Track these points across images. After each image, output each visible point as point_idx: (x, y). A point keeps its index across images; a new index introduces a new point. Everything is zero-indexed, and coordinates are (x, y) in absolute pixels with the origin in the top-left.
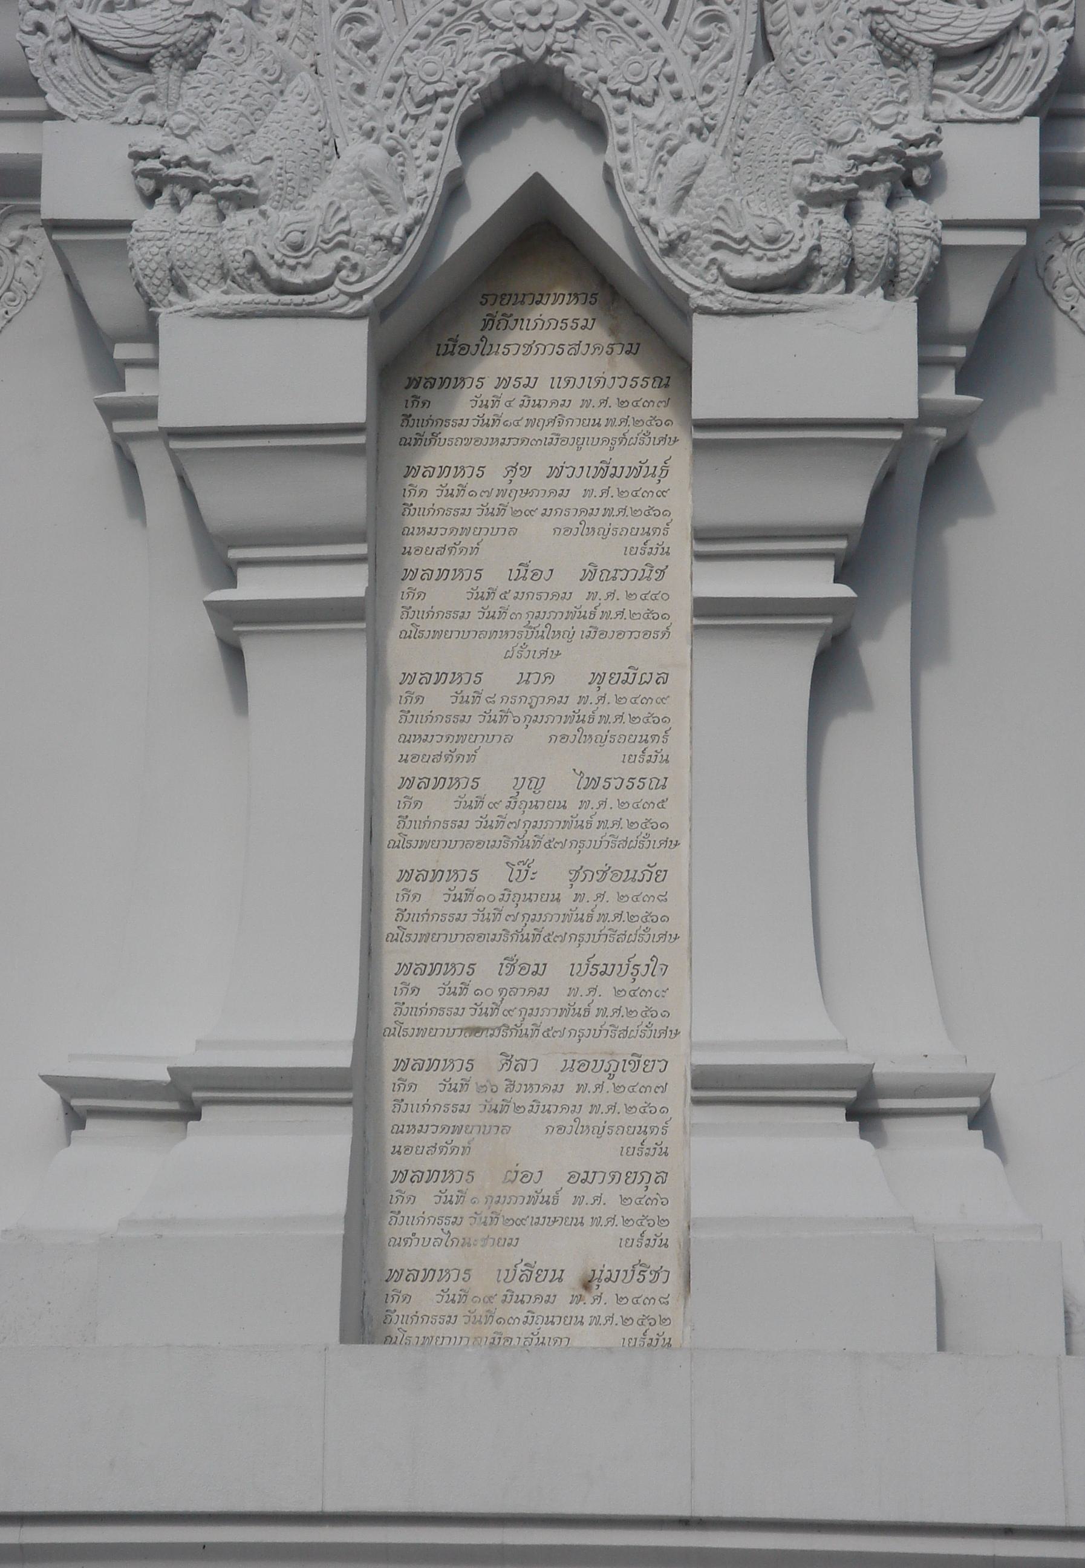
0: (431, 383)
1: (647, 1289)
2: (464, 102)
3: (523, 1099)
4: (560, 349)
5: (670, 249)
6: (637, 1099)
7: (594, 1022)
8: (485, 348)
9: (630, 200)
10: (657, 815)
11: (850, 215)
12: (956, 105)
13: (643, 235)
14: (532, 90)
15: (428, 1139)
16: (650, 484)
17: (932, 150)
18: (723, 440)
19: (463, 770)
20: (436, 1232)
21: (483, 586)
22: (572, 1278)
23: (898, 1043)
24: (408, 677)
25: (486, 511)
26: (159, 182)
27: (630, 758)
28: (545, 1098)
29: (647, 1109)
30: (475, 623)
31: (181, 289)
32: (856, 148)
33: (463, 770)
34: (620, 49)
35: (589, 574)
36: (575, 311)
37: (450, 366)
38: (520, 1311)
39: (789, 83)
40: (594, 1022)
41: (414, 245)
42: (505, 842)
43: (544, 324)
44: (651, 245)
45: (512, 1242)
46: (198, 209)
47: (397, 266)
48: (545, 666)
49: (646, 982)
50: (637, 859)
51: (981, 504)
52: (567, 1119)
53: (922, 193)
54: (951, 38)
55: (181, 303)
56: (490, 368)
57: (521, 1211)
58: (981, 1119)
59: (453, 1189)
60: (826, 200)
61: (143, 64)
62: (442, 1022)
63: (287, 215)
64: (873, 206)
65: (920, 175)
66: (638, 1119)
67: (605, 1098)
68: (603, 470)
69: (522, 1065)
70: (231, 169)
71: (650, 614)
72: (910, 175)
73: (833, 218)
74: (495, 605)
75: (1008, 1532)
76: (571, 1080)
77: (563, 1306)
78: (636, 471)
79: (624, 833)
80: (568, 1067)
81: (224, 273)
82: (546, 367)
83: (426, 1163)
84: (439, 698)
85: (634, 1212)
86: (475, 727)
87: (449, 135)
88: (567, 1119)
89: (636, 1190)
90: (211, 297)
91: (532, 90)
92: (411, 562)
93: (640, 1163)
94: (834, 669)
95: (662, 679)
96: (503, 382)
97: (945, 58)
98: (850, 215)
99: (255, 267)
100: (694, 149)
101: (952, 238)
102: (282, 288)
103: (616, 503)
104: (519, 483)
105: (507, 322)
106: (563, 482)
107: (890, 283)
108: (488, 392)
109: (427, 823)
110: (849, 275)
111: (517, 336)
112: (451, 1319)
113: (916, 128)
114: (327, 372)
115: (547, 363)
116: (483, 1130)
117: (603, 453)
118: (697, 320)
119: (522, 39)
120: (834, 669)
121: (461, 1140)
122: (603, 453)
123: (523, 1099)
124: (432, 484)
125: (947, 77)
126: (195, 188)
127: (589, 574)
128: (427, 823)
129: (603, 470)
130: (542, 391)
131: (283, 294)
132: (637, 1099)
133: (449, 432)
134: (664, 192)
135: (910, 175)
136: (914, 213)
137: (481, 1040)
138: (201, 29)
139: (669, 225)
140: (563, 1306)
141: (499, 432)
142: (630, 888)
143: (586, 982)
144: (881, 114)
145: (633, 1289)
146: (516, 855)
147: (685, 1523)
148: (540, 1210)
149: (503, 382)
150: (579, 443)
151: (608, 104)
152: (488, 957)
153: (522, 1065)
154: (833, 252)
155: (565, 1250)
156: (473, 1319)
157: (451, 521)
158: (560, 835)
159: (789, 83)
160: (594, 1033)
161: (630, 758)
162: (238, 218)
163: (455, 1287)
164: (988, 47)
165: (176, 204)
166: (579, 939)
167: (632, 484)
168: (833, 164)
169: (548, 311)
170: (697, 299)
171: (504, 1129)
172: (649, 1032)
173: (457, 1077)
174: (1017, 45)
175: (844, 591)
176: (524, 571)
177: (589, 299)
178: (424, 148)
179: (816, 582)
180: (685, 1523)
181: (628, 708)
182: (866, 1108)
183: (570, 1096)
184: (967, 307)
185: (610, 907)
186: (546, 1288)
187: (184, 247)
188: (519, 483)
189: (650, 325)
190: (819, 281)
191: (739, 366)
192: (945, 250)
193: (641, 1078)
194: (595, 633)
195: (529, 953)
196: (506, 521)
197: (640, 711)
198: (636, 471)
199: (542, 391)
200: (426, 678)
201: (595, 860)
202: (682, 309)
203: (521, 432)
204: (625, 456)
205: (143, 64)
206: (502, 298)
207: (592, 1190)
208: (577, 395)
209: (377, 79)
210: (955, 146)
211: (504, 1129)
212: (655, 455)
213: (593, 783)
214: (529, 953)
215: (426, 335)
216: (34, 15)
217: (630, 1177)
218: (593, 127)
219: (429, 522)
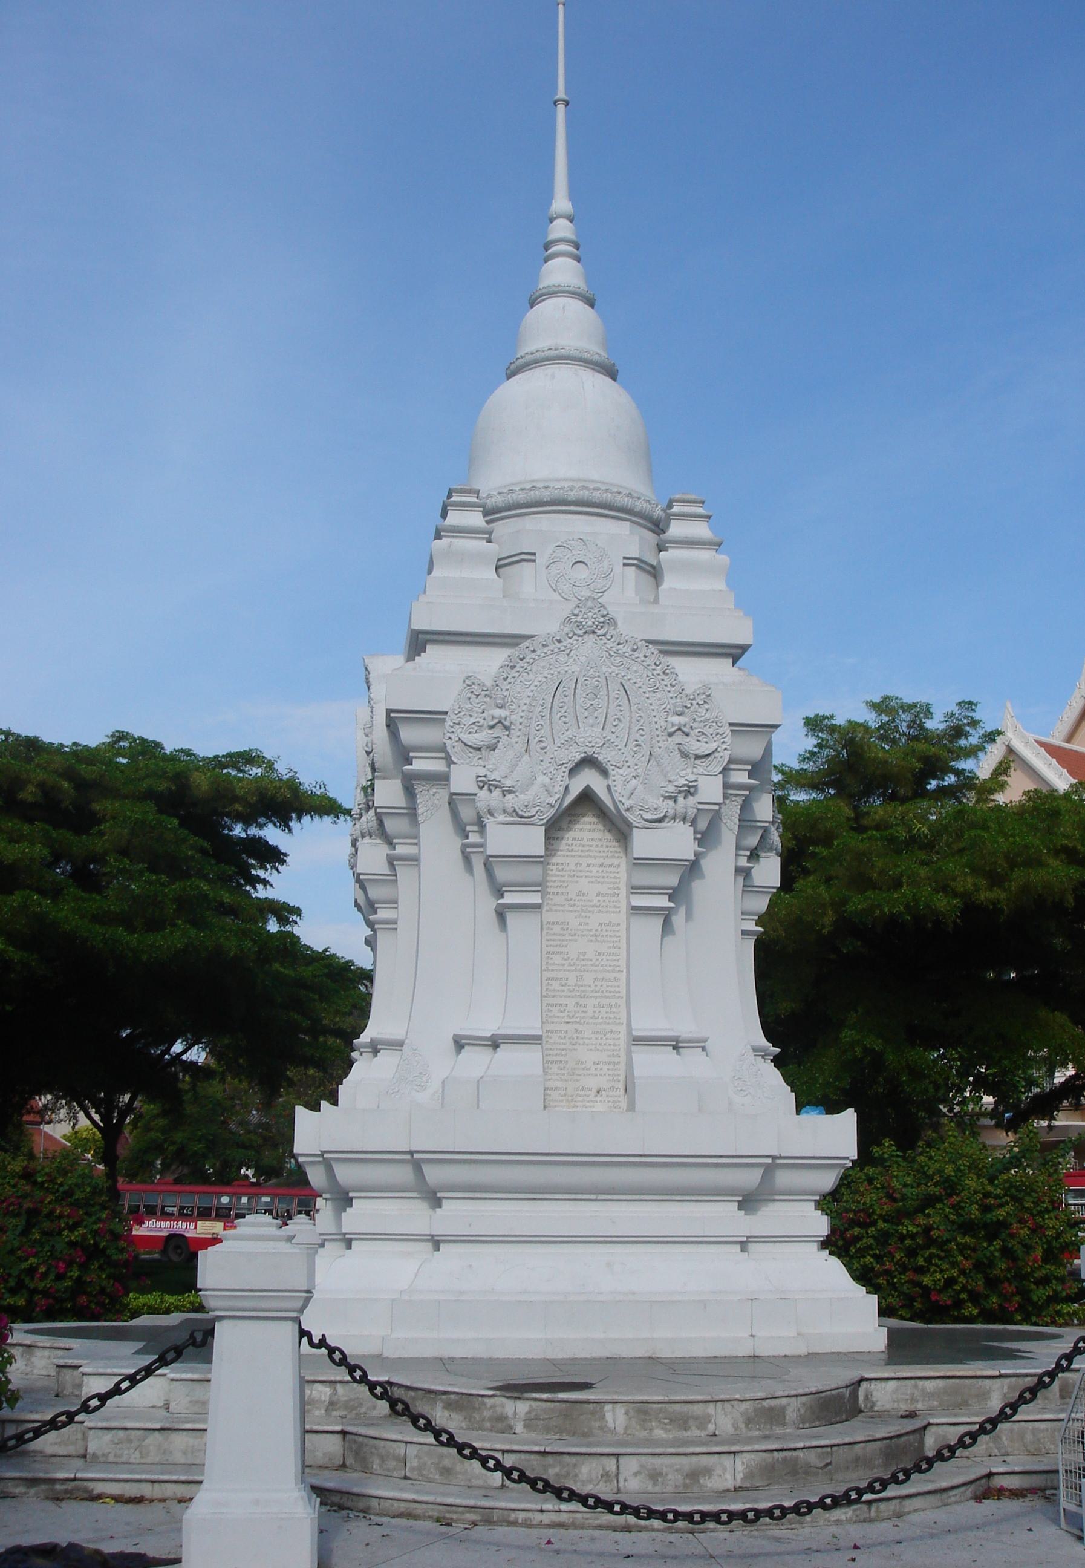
0: (554, 839)
1: (615, 1093)
2: (570, 765)
3: (581, 1042)
4: (590, 830)
5: (628, 810)
6: (612, 1042)
7: (600, 1020)
8: (569, 829)
9: (616, 795)
10: (616, 963)
11: (675, 802)
12: (701, 770)
13: (620, 805)
14: (589, 762)
15: (555, 1052)
16: (615, 870)
17: (489, 518)
18: (641, 863)
19: (564, 949)
20: (556, 1077)
21: (569, 897)
22: (594, 1090)
23: (684, 1029)
24: (548, 923)
25: (569, 876)
26: (484, 783)
27: (609, 947)
28: (587, 1041)
29: (614, 1045)
30: (567, 908)
31: (491, 814)
32: (676, 784)
33: (564, 949)
34: (613, 753)
35: (598, 895)
36: (594, 819)
37: (559, 834)
38: (581, 1099)
39: (659, 765)
40: (600, 1020)
41: (557, 805)
42: (576, 970)
43: (585, 823)
44: (622, 808)
45: (578, 1081)
46: (497, 793)
47: (553, 811)
48: (587, 920)
49: (614, 1010)
50: (613, 975)
51: (702, 876)
52: (593, 1047)
53: (692, 795)
54: (699, 752)
55: (492, 819)
56: (570, 835)
57: (581, 1072)
58: (704, 1049)
59: (562, 1066)
60: (670, 798)
61: (479, 749)
62: (556, 1020)
63: (522, 796)
64: (681, 799)
65: (692, 790)
66: (612, 1047)
67: (603, 1042)
68: (602, 865)
69: (580, 1032)
70: (508, 783)
71: (615, 907)
72: (690, 791)
73: (671, 803)
74: (572, 902)
75: (721, 1157)
76: (594, 1036)
77: (592, 1098)
78: (610, 866)
79: (608, 968)
80: (593, 1033)
81: (505, 811)
82: (586, 835)
83: (555, 1059)
84: (557, 929)
85: (611, 1072)
86: (567, 937)
87: (566, 774)
88: (593, 1047)
89: (611, 1067)
90: (501, 818)
91: (589, 762)
92: (548, 890)
93: (613, 1059)
94: (667, 927)
95: (618, 925)
96: (574, 839)
97: (697, 757)
98: (675, 802)
99: (515, 811)
100: (634, 781)
101: (701, 806)
102: (522, 817)
103: (605, 875)
104: (579, 868)
105: (575, 822)
106: (590, 868)
107: (684, 819)
108: (570, 842)
109: (554, 964)
110: (674, 818)
111: (577, 826)
112: (562, 1101)
113: (692, 778)
114: (533, 841)
115: (587, 832)
116: (570, 1050)
117: (601, 860)
118: (635, 830)
119: (587, 749)
120: (667, 927)
121: (563, 1053)
122: (601, 860)
123: (581, 1042)
124: (554, 868)
125: (698, 762)
126: (496, 787)
127: (598, 895)
128: (554, 964)
129: (602, 865)
130: (585, 842)
131: (521, 818)
132: (612, 1042)
133: (559, 853)
134: (626, 793)
135: (690, 791)
136: (691, 800)
137: (569, 1025)
138: (495, 741)
139: (628, 803)
140: (592, 1098)
141: (573, 853)
142: (610, 984)
143: (597, 1010)
144: (683, 774)
145: (611, 1093)
146: (578, 974)
147: (641, 1156)
148: (585, 1072)
149: (574, 839)
150: (595, 857)
151: (610, 768)
152: (571, 1002)
153: (580, 1032)
154: (671, 812)
155: (593, 1083)
156: (567, 1100)
157: (559, 878)
158: (591, 968)
159: (659, 765)
160: (600, 1024)
161: (609, 947)
162: (509, 797)
163: (563, 1092)
164: (709, 755)
165: (490, 791)
166: (596, 997)
167: (610, 869)
168: (671, 788)
169: (586, 819)
170: (635, 824)
171: (575, 1050)
172: (615, 1023)
173: (563, 1035)
174: (717, 754)
175: (672, 905)
176: (580, 893)
177: (598, 816)
178: (559, 778)
179: (663, 902)
180: (641, 1156)
181: (609, 933)
182: (677, 1045)
183: (594, 1041)
184: (702, 825)
185: (604, 989)
186: (587, 1093)
187: (494, 804)
188: (579, 868)
189: (619, 829)
190: (667, 820)
191: (644, 843)
192: (698, 810)
193: (612, 1036)
194: (599, 912)
195: (582, 1001)
196: (575, 878)
197: (612, 934)
198: (610, 866)
199: (585, 842)
200: (553, 923)
201: (600, 976)
202: (629, 825)
203: (579, 853)
204: (608, 862)
205: (479, 749)
206: (574, 815)
207: (599, 1067)
208: (594, 843)
209: (547, 758)
210: (702, 782)
211: (575, 1050)
212: (616, 862)
213: (599, 954)
214: (582, 1001)
215: (556, 827)
216: (449, 735)
217: (610, 1063)
218: (605, 773)
219: (554, 879)
